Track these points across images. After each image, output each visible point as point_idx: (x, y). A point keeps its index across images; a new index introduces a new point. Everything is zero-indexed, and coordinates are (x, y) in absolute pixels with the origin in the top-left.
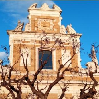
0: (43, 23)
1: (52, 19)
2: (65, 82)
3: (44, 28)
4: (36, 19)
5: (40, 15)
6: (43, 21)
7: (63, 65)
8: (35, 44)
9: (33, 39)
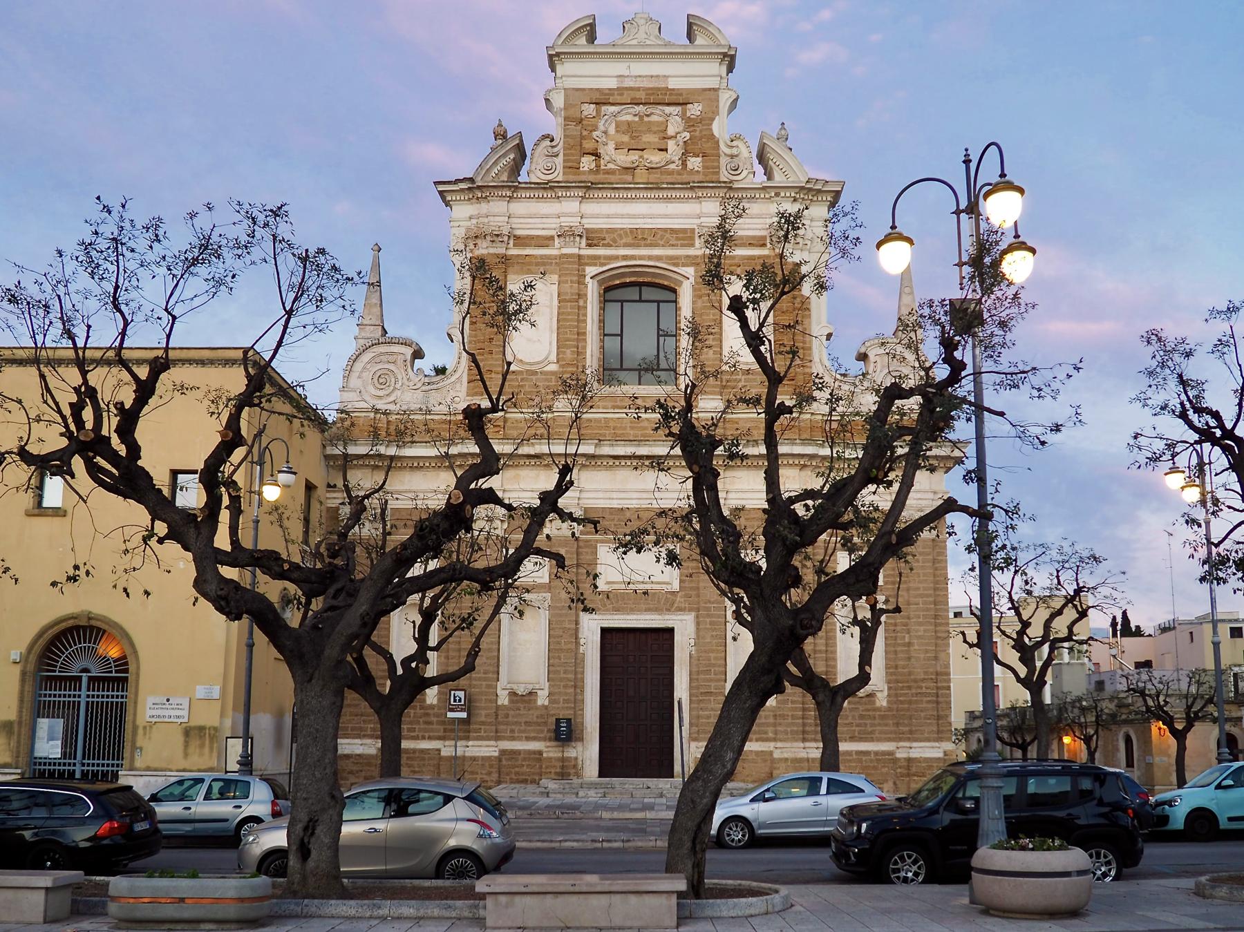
0: (628, 128)
1: (680, 100)
3: (634, 156)
4: (590, 110)
5: (612, 84)
6: (629, 118)
8: (583, 252)
9: (574, 221)
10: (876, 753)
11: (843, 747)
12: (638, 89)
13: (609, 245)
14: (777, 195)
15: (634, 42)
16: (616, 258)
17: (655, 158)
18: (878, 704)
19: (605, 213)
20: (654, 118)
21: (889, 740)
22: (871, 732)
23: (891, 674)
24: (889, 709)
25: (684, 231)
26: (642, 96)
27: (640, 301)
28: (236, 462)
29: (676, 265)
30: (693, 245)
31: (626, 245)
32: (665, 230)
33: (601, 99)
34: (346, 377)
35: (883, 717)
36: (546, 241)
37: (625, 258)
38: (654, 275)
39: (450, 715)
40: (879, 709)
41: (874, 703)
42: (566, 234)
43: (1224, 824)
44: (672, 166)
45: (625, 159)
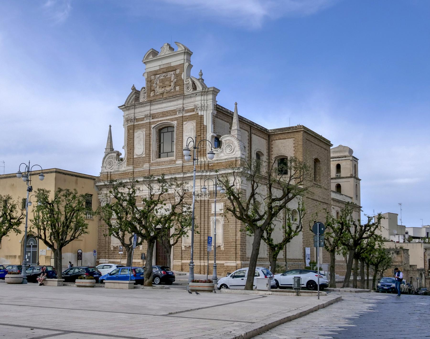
0: (162, 81)
1: (174, 69)
2: (354, 231)
3: (163, 89)
4: (153, 77)
5: (158, 68)
6: (162, 78)
7: (423, 267)
8: (151, 121)
9: (148, 113)
10: (220, 264)
11: (134, 261)
12: (164, 68)
13: (157, 118)
14: (196, 95)
15: (163, 54)
16: (158, 121)
17: (168, 89)
18: (222, 249)
19: (157, 108)
20: (168, 76)
21: (224, 260)
22: (220, 258)
23: (225, 240)
24: (225, 251)
25: (174, 110)
26: (165, 70)
27: (168, 132)
28: (320, 145)
29: (172, 121)
30: (176, 114)
31: (161, 117)
32: (170, 111)
33: (155, 73)
34: (103, 163)
35: (222, 253)
36: (142, 119)
37: (161, 121)
38: (161, 126)
39: (119, 253)
40: (221, 251)
41: (220, 249)
42: (146, 116)
43: (280, 285)
44: (172, 90)
45: (161, 90)
